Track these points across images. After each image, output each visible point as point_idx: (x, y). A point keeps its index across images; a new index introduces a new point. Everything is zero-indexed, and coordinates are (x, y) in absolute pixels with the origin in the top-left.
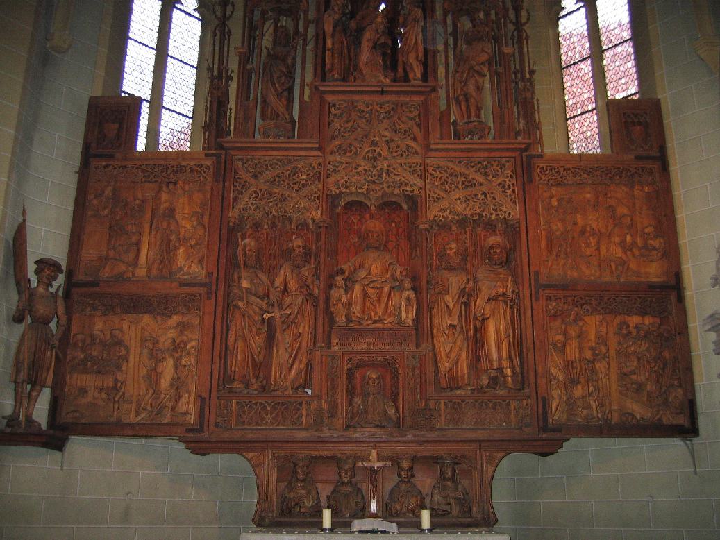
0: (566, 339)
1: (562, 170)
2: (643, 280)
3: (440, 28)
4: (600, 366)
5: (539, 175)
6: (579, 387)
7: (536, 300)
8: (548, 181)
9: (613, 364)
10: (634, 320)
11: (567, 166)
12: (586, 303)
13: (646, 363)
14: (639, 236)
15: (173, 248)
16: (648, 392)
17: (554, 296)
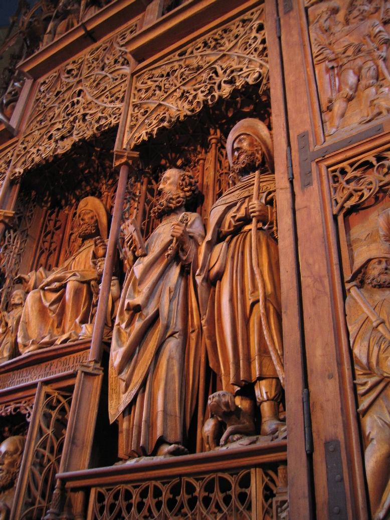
17: (351, 165)
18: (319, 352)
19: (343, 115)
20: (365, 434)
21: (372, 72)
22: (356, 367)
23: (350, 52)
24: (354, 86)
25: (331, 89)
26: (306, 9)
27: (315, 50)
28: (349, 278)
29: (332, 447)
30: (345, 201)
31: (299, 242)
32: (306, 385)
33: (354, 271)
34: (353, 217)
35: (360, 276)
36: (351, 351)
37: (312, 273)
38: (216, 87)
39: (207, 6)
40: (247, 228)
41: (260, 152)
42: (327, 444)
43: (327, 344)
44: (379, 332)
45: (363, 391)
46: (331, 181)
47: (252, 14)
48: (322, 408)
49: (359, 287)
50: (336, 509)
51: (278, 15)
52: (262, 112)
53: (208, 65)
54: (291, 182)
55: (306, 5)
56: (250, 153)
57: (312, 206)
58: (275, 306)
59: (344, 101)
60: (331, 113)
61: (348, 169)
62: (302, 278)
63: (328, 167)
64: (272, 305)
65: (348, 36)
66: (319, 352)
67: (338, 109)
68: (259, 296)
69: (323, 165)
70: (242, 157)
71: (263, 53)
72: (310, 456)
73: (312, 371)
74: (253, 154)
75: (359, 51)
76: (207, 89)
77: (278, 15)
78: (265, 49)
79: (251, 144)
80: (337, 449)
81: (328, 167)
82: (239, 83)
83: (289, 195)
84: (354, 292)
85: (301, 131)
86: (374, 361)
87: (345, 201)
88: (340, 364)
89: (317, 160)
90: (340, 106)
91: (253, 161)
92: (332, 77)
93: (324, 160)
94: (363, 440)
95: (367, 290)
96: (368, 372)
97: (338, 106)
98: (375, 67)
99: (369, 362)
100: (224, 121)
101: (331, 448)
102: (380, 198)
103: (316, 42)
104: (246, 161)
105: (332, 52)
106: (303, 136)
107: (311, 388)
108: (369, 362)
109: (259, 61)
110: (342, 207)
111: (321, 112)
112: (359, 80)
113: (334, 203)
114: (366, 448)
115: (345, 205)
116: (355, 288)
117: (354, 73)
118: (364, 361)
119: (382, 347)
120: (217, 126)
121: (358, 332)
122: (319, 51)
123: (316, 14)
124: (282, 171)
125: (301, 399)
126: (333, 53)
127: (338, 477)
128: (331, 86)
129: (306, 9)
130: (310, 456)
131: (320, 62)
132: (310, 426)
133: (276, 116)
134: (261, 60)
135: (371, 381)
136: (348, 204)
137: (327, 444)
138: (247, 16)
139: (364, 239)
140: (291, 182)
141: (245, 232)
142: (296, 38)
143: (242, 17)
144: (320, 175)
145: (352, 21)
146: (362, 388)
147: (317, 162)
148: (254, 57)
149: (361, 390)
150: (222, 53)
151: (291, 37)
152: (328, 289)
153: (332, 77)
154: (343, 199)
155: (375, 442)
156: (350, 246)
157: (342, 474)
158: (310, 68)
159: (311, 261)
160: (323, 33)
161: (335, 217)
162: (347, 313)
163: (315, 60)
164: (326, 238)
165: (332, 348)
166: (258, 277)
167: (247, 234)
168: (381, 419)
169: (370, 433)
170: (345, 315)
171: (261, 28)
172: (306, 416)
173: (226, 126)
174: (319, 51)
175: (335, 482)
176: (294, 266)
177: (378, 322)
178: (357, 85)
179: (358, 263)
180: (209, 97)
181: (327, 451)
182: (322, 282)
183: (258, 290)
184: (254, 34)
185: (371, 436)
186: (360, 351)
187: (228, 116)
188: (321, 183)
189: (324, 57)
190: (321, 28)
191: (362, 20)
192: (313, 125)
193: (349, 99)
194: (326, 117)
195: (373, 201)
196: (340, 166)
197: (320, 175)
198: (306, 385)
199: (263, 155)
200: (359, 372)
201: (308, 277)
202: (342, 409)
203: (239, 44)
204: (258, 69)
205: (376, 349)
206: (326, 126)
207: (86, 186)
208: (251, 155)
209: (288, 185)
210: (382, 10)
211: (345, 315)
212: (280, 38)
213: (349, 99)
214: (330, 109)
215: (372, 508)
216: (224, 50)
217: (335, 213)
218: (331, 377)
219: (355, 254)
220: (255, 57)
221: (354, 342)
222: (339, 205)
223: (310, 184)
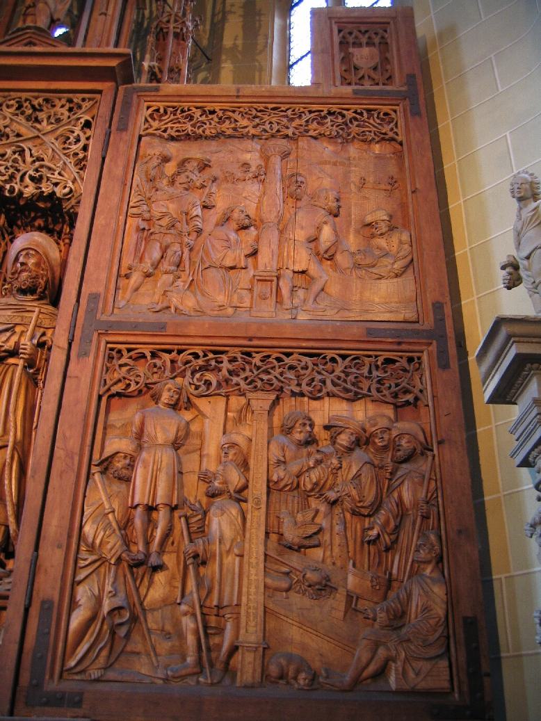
0: (140, 448)
1: (199, 112)
2: (353, 316)
3: (283, 507)
4: (222, 522)
5: (146, 120)
6: (160, 577)
7: (79, 356)
8: (165, 131)
9: (257, 518)
10: (325, 411)
11: (209, 107)
12: (205, 368)
13: (348, 515)
14: (352, 230)
15: (225, 485)
16: (349, 597)
17: (129, 350)
18: (55, 522)
19: (137, 289)
20: (75, 599)
21: (176, 259)
22: (82, 543)
23: (164, 222)
24: (156, 263)
25: (135, 254)
26: (140, 137)
27: (134, 200)
28: (96, 463)
29: (47, 606)
30: (112, 385)
31: (62, 411)
32: (37, 548)
33: (103, 458)
34: (115, 401)
35: (105, 464)
36: (81, 527)
37: (66, 447)
38: (18, 176)
39: (37, 65)
40: (11, 361)
41: (45, 279)
42: (43, 602)
43: (63, 518)
44: (108, 519)
45: (83, 565)
46: (106, 360)
47: (83, 100)
48: (46, 570)
49: (101, 473)
50: (39, 655)
51: (110, 127)
52: (58, 215)
53: (16, 139)
54: (70, 344)
55: (142, 133)
56: (34, 274)
57: (83, 379)
58: (21, 456)
59: (142, 275)
60: (127, 281)
61: (125, 353)
62: (56, 448)
63: (108, 343)
64: (18, 453)
65: (168, 202)
66: (55, 522)
67: (135, 282)
68: (8, 442)
69: (104, 339)
70: (25, 274)
71: (81, 164)
72: (27, 610)
73: (45, 537)
74: (36, 277)
75: (173, 226)
76: (7, 174)
77: (110, 127)
78: (85, 158)
79: (38, 265)
80: (50, 609)
81: (108, 343)
82: (46, 188)
83: (64, 357)
84: (97, 477)
85: (94, 290)
86: (98, 541)
87: (112, 385)
88: (70, 537)
89: (99, 331)
90: (137, 279)
91: (34, 286)
92: (140, 240)
93: (106, 334)
94: (73, 604)
95: (108, 478)
96: (91, 549)
97: (136, 278)
98: (180, 253)
99: (93, 542)
100: (13, 207)
101: (46, 606)
102: (143, 392)
103: (137, 189)
104: (28, 283)
105: (148, 209)
106: (94, 297)
107: (41, 552)
108: (93, 542)
109: (74, 170)
110: (109, 389)
111: (119, 275)
112: (162, 257)
113: (103, 382)
114: (74, 610)
115: (112, 388)
116: (99, 474)
117: (161, 247)
118: (90, 540)
119: (107, 533)
120: (4, 210)
121: (116, 681)
122: (138, 202)
123: (148, 152)
124: (64, 328)
125: (30, 560)
126: (149, 211)
127: (46, 630)
128: (136, 250)
129: (140, 137)
130: (27, 610)
131: (134, 216)
132: (33, 585)
133: (74, 258)
134: (78, 172)
135: (92, 558)
136: (115, 389)
137: (43, 602)
138: (77, 98)
139: (118, 426)
140: (70, 344)
141: (7, 364)
142: (119, 171)
143: (70, 95)
144: (98, 349)
145: (177, 184)
146: (82, 562)
147: (99, 334)
148: (71, 162)
149: (82, 563)
150: (36, 133)
151: (115, 167)
152: (76, 467)
153: (140, 240)
154: (112, 382)
155: (82, 608)
156: (105, 428)
157: (50, 630)
158: (122, 218)
159: (68, 434)
160: (148, 181)
161: (100, 397)
162: (87, 494)
163: (131, 211)
164: (86, 415)
165: (66, 523)
166: (11, 415)
167: (9, 368)
168: (91, 591)
169: (80, 600)
170: (85, 496)
171: (87, 125)
172: (31, 576)
173: (13, 213)
174: (138, 202)
175: (42, 634)
176: (51, 434)
177: (110, 510)
178: (159, 262)
179: (108, 452)
180: (8, 186)
181: (42, 608)
182: (72, 458)
183: (9, 434)
184: (77, 131)
185: (80, 603)
186: (88, 529)
187: (19, 204)
188: (96, 357)
189: (140, 212)
190: (147, 173)
191: (187, 189)
192: (107, 288)
193: (148, 275)
194: (122, 282)
195: (136, 393)
196: (119, 346)
197: (98, 349)
198: (37, 548)
199: (47, 282)
200: (83, 548)
201: (62, 449)
202: (62, 576)
203: (59, 132)
204: (70, 184)
205: (102, 533)
206: (118, 293)
208: (34, 278)
209: (66, 346)
210: (207, 190)
211: (85, 496)
212: (104, 159)
213: (148, 275)
214: (127, 276)
215: (66, 657)
216: (38, 130)
217: (100, 393)
218: (59, 547)
219: (107, 443)
220: (70, 162)
221: (86, 522)
222: (106, 387)
223: (86, 354)
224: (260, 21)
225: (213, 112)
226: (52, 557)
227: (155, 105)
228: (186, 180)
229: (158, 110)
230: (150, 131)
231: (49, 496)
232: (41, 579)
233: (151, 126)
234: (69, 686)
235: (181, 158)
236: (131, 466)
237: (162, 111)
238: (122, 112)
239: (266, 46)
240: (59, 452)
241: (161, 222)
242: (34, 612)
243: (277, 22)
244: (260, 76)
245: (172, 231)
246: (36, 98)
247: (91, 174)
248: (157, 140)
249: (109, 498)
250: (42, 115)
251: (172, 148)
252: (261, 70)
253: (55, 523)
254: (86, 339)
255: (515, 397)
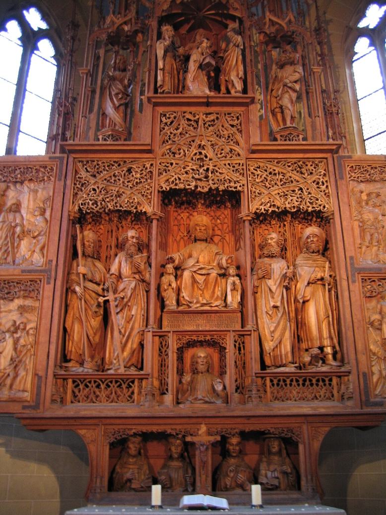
5: (349, 173)
11: (374, 166)
17: (369, 279)
18: (360, 345)
138: (317, 161)
142: (346, 200)
207: (183, 197)
209: (346, 278)
224: (338, 72)
225: (376, 168)
226: (363, 358)
227: (351, 165)
228: (372, 203)
229: (352, 167)
230: (352, 178)
231: (356, 336)
232: (360, 366)
233: (352, 176)
234: (377, 400)
235: (367, 192)
236: (381, 324)
237: (354, 168)
238: (339, 170)
239: (344, 88)
240: (355, 320)
241: (368, 223)
242: (361, 377)
243: (347, 71)
244: (345, 107)
245: (373, 227)
246: (299, 161)
247: (333, 199)
248: (355, 183)
249: (376, 335)
250: (303, 170)
251: (362, 186)
252: (345, 103)
253: (360, 346)
254: (353, 275)
255: (88, 109)
